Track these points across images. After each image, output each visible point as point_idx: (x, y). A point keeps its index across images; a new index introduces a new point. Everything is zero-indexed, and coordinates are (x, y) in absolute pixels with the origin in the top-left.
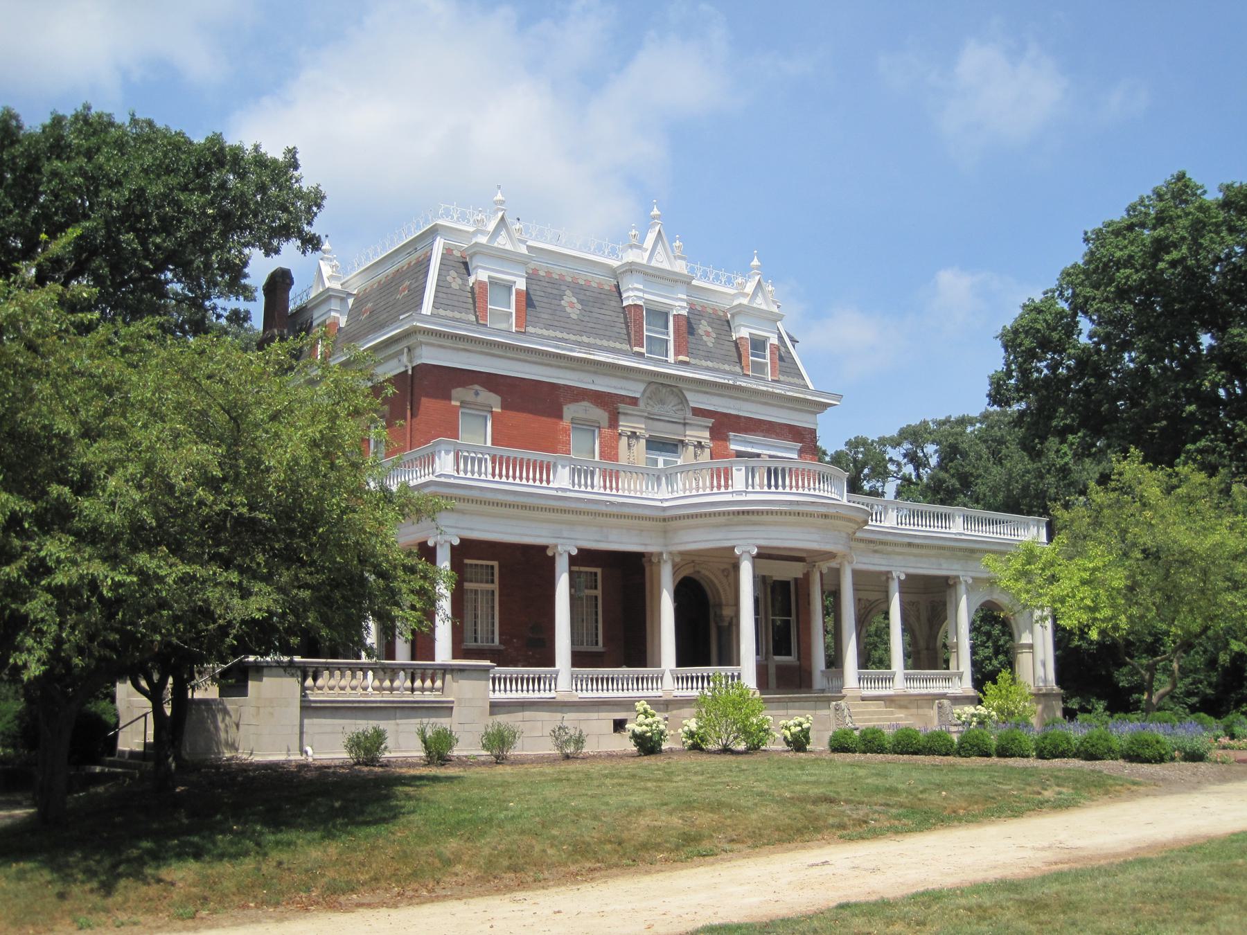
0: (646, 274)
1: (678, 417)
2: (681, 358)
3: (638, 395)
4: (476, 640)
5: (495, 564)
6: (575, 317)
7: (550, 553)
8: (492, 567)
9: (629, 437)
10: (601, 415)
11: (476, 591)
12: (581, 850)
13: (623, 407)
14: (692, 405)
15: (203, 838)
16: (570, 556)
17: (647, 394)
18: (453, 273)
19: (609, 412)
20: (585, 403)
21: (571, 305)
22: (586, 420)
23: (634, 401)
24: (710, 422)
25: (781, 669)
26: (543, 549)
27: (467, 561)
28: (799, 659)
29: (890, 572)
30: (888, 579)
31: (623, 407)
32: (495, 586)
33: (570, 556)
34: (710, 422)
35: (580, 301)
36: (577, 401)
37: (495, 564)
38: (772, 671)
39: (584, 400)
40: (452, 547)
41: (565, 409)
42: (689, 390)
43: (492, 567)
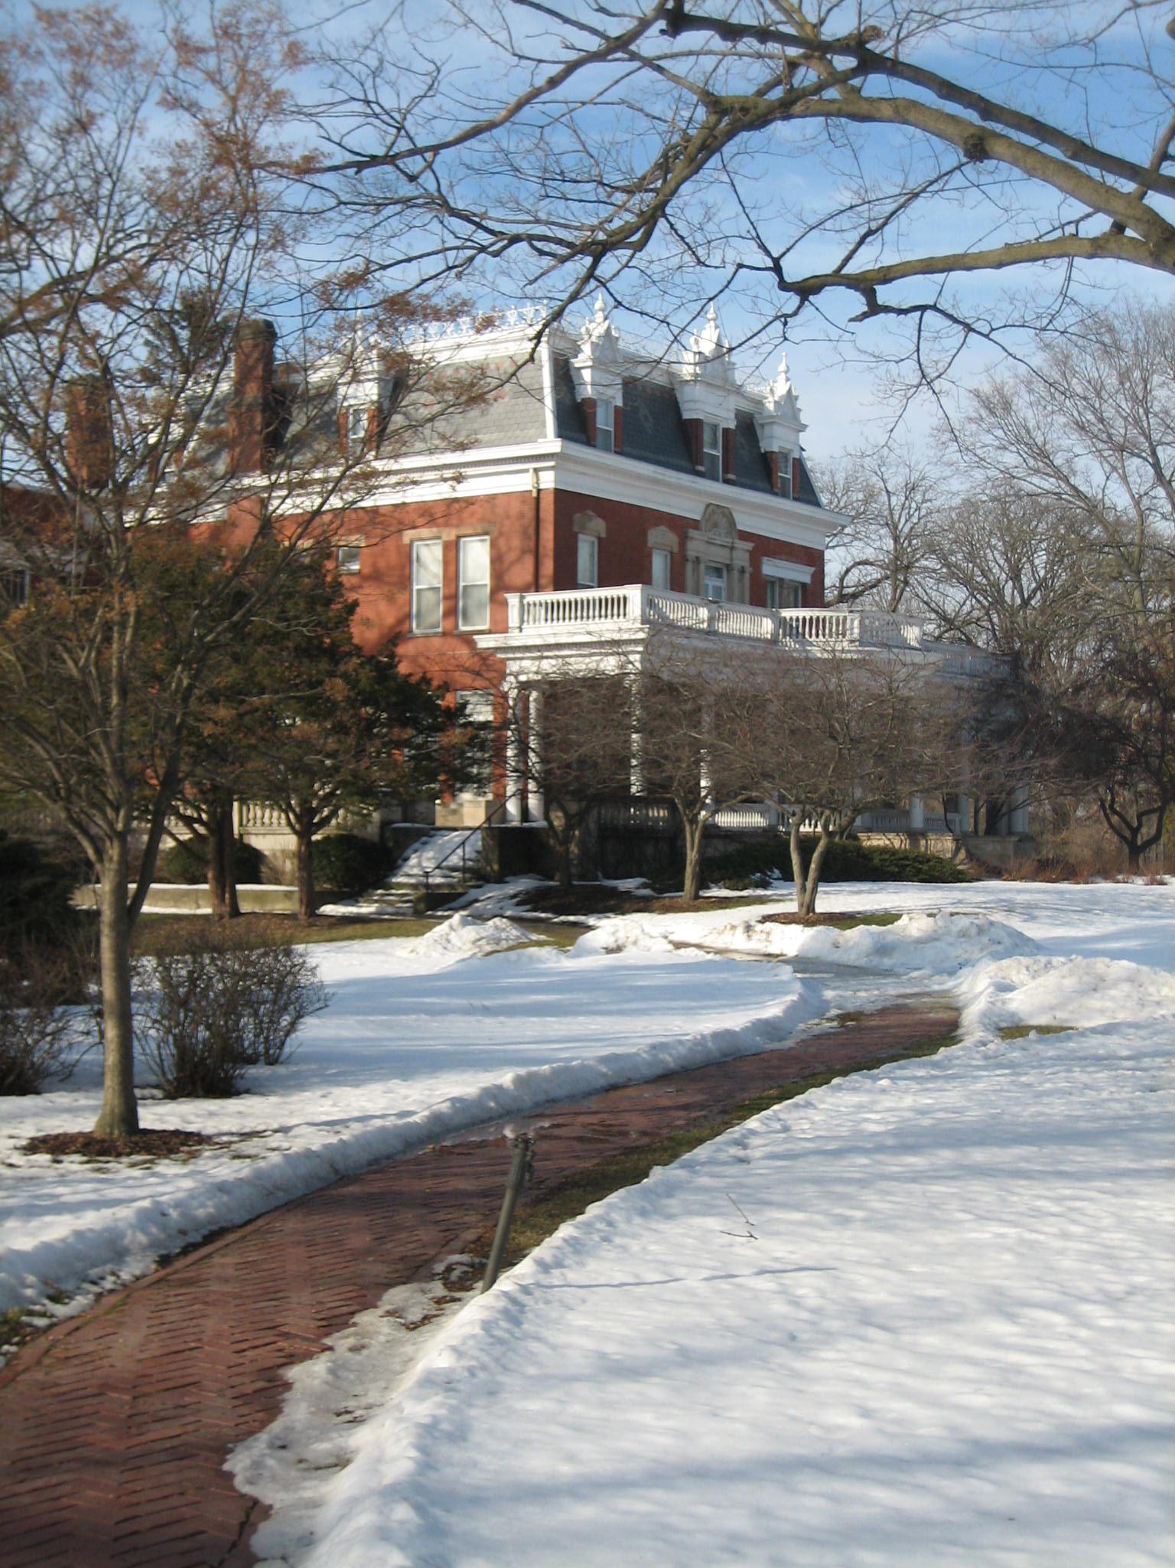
3: (697, 517)
14: (739, 527)
20: (663, 528)
24: (750, 546)
34: (750, 546)
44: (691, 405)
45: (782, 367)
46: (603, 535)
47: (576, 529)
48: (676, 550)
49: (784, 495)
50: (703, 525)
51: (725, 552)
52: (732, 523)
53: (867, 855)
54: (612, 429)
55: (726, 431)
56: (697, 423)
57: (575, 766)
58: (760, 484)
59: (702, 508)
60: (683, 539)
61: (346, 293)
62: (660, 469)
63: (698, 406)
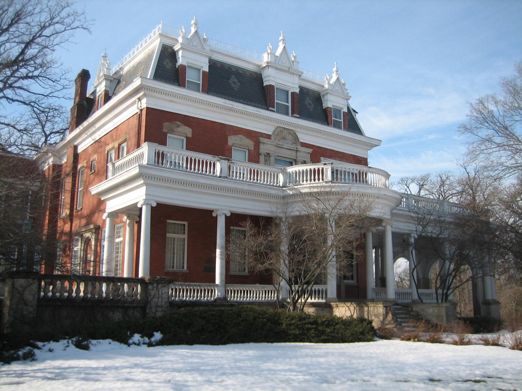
0: (276, 69)
1: (293, 147)
2: (295, 115)
3: (270, 133)
4: (173, 267)
5: (186, 223)
6: (236, 89)
7: (214, 215)
8: (184, 225)
9: (265, 156)
10: (250, 144)
11: (174, 239)
12: (318, 336)
13: (262, 139)
14: (301, 140)
15: (162, 356)
16: (226, 216)
17: (276, 133)
18: (167, 60)
19: (254, 142)
20: (241, 136)
21: (235, 83)
22: (240, 145)
23: (268, 137)
24: (310, 151)
25: (348, 287)
26: (210, 212)
27: (168, 221)
28: (357, 282)
29: (410, 234)
30: (408, 237)
31: (262, 139)
32: (186, 236)
33: (226, 216)
34: (310, 151)
35: (239, 81)
36: (236, 134)
37: (186, 223)
38: (343, 288)
39: (240, 134)
40: (152, 207)
41: (229, 138)
42: (299, 132)
43: (184, 225)
44: (267, 78)
45: (335, 69)
46: (190, 135)
47: (165, 130)
48: (252, 148)
49: (339, 128)
50: (273, 138)
51: (294, 153)
52: (296, 138)
53: (335, 322)
54: (201, 83)
55: (293, 93)
56: (271, 87)
57: (448, 250)
58: (263, 107)
59: (273, 129)
60: (257, 144)
61: (498, 149)
62: (228, 102)
63: (270, 78)
